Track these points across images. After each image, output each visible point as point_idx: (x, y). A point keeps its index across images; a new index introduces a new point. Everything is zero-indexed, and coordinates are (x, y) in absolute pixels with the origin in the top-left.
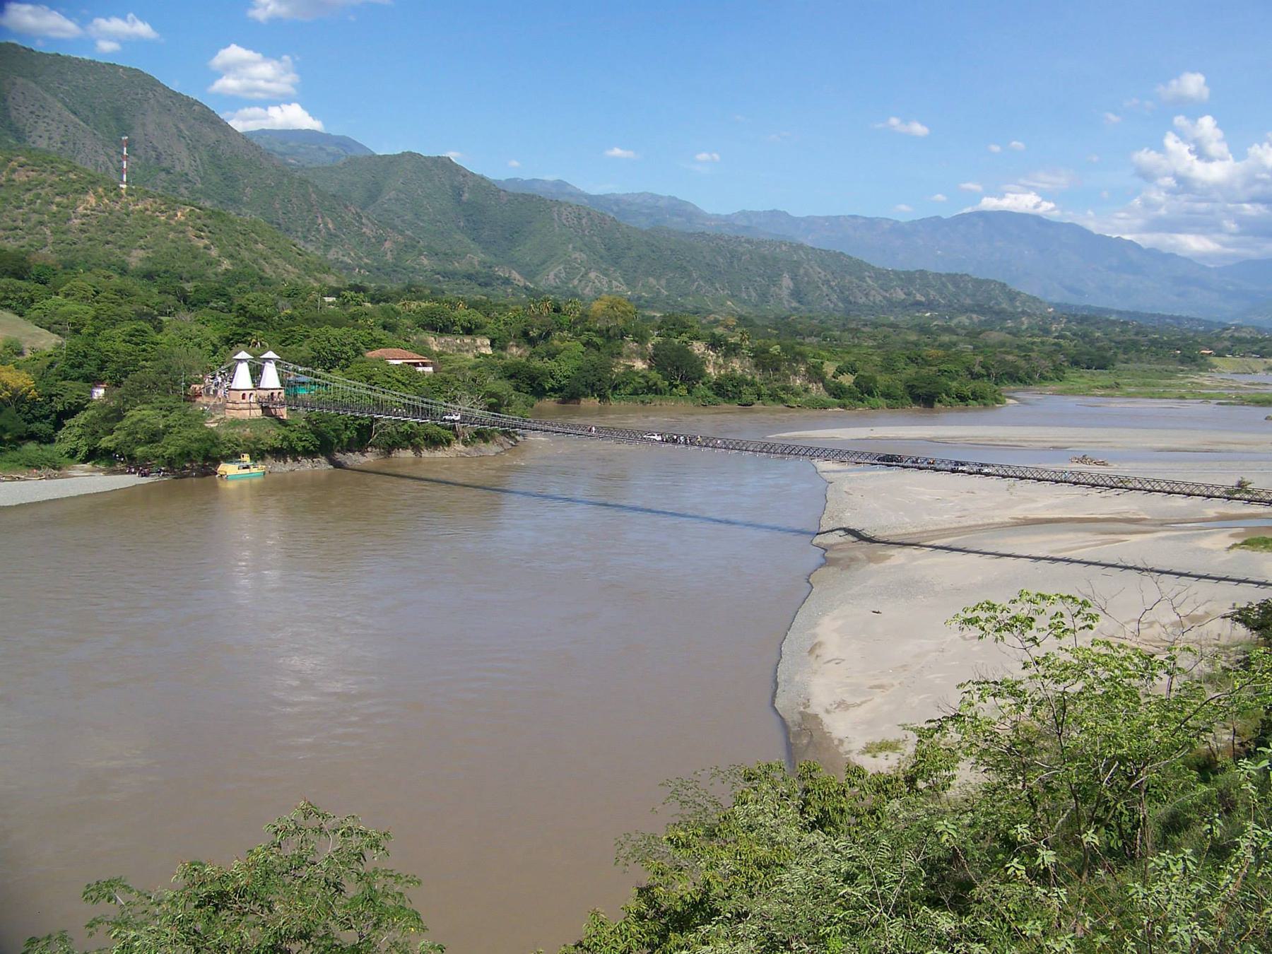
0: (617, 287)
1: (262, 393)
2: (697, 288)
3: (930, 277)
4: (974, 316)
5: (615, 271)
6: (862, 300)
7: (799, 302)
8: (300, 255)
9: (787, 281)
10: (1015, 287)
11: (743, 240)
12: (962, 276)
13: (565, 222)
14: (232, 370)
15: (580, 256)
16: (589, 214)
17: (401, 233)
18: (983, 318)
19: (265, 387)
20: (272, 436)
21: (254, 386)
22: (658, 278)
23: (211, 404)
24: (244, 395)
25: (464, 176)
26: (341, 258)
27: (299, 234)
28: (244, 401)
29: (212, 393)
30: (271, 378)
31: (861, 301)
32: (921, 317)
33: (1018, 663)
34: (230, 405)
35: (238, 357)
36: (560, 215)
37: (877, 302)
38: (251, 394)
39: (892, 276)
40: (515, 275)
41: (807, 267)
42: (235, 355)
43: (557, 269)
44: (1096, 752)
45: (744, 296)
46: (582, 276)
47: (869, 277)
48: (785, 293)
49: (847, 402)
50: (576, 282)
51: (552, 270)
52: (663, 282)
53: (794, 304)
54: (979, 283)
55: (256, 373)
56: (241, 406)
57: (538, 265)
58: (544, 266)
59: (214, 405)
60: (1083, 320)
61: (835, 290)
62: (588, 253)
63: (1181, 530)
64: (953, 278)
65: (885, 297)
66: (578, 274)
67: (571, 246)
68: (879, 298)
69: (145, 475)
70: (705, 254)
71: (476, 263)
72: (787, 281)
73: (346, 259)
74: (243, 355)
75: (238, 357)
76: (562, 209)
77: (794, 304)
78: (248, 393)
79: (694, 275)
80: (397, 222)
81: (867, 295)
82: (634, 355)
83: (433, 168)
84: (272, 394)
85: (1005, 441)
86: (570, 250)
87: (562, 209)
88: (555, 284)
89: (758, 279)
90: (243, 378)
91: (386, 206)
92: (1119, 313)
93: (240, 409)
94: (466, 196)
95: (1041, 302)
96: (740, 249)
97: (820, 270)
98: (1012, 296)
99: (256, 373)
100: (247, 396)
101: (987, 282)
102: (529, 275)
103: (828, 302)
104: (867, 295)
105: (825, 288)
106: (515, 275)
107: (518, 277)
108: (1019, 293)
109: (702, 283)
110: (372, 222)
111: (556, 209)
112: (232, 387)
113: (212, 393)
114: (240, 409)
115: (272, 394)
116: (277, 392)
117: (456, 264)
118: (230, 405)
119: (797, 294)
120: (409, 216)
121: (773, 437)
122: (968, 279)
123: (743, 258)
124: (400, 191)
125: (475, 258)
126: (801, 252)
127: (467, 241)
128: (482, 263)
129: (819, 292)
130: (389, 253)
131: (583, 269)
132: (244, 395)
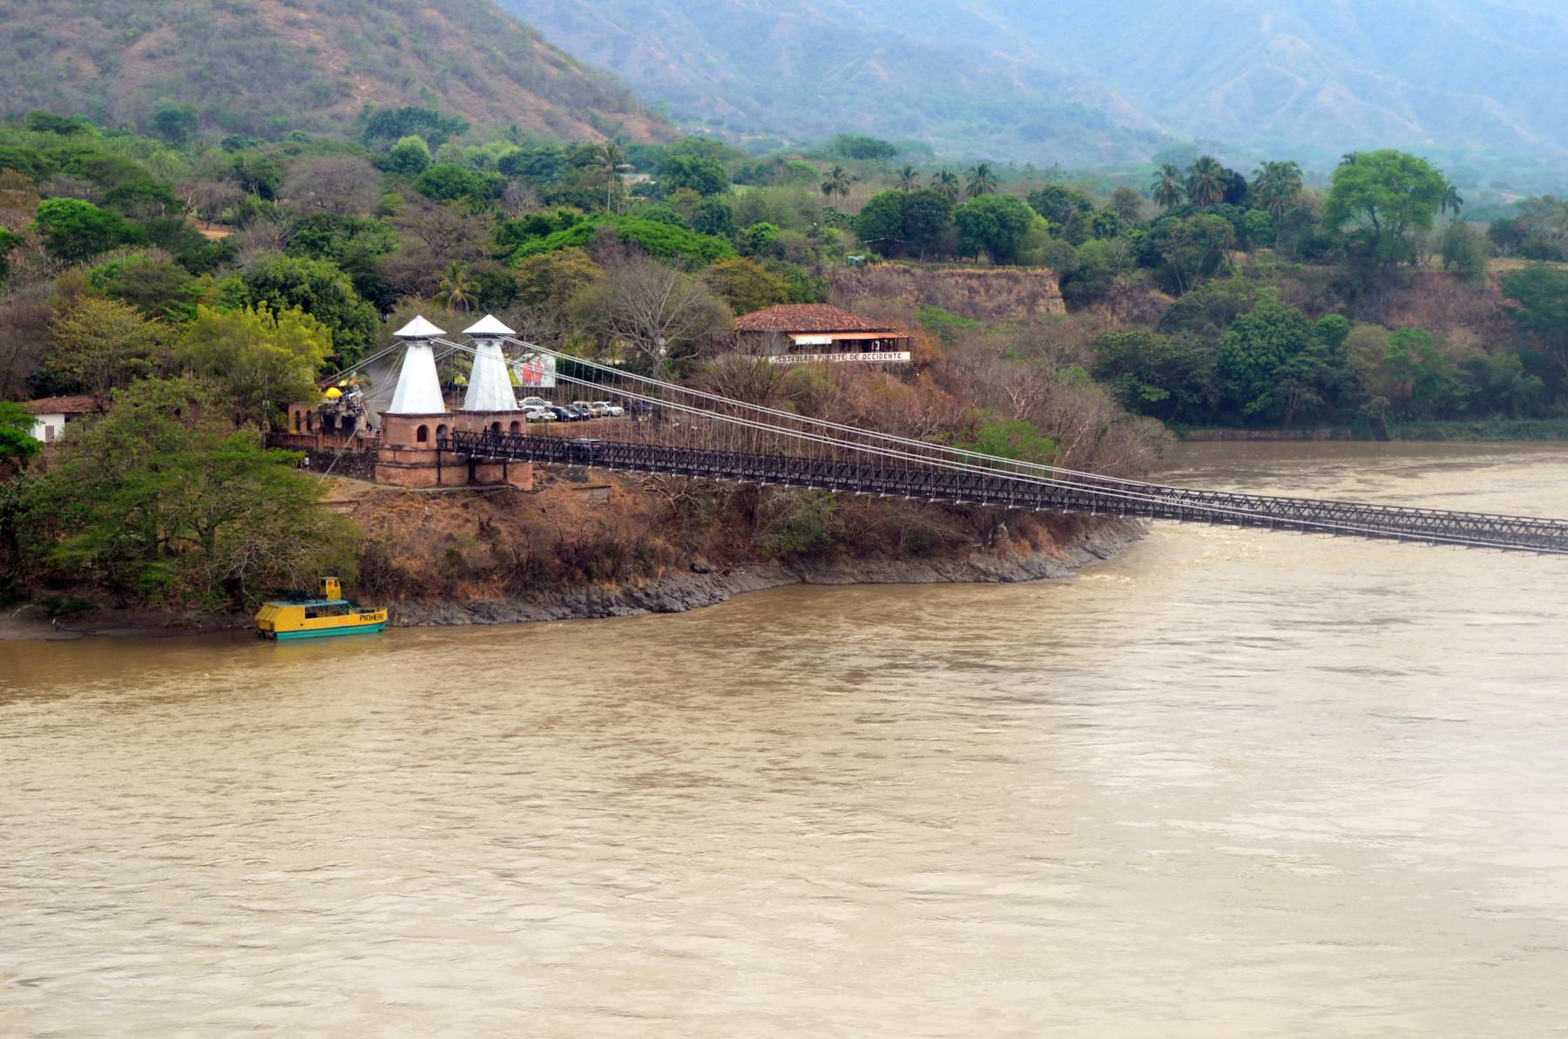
14: (392, 360)
19: (478, 407)
23: (339, 454)
27: (135, 451)
28: (422, 445)
29: (338, 425)
35: (406, 331)
42: (400, 327)
44: (1337, 286)
49: (1118, 335)
56: (415, 458)
59: (345, 457)
63: (1018, 920)
69: (119, 694)
74: (419, 326)
75: (406, 331)
82: (841, 548)
85: (926, 900)
100: (432, 431)
113: (338, 425)
115: (496, 426)
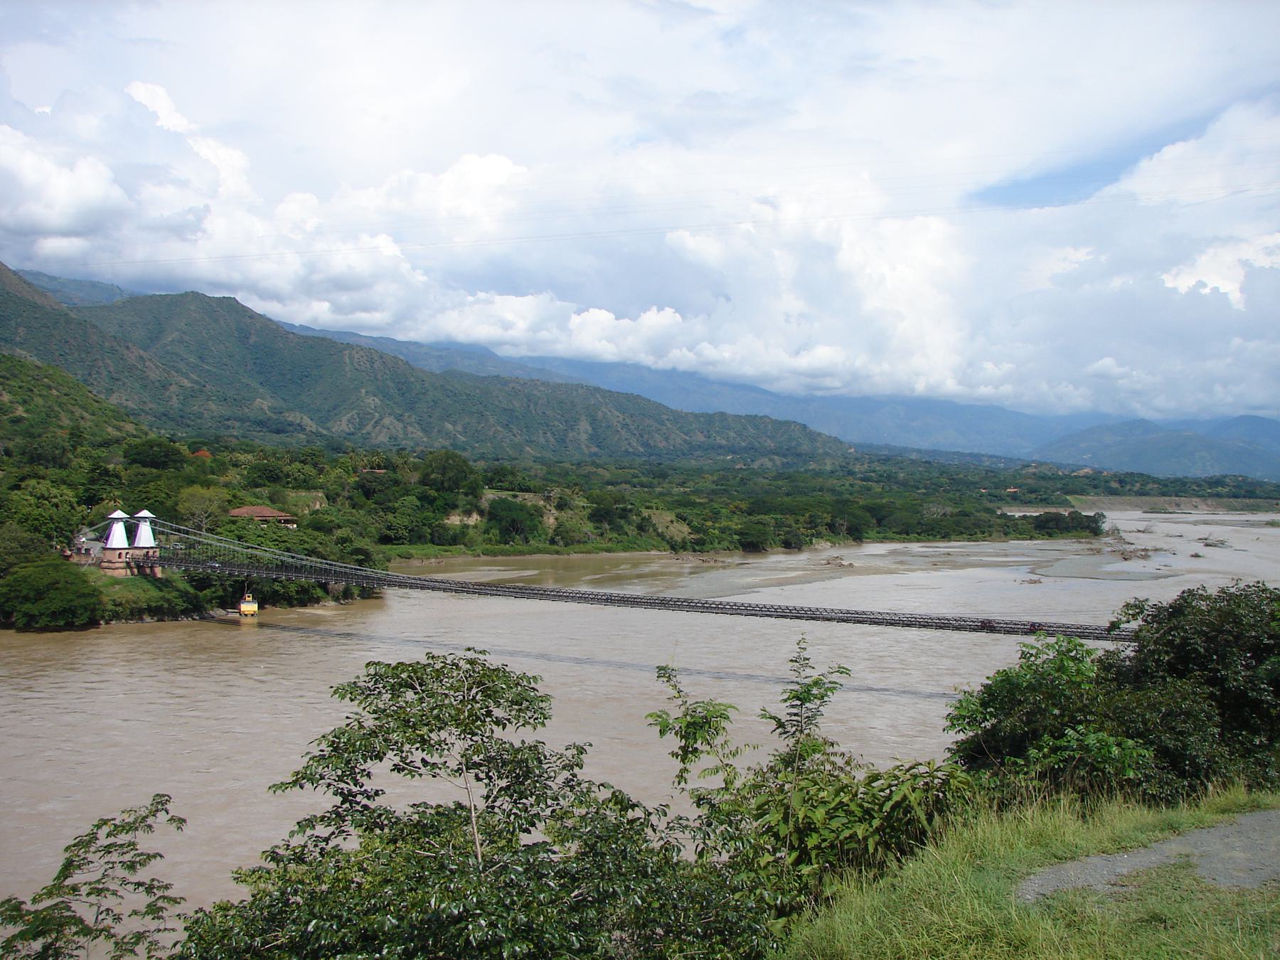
0: (412, 433)
1: (137, 552)
2: (494, 433)
3: (730, 419)
4: (776, 457)
5: (409, 417)
6: (662, 444)
7: (598, 446)
8: (97, 402)
9: (584, 426)
10: (814, 427)
11: (539, 383)
12: (761, 418)
13: (357, 366)
15: (372, 401)
16: (382, 358)
17: (187, 376)
18: (785, 460)
19: (141, 546)
20: (151, 594)
21: (129, 545)
22: (454, 424)
24: (120, 554)
25: (251, 317)
26: (125, 403)
28: (120, 560)
30: (146, 537)
31: (661, 445)
32: (723, 461)
33: (856, 675)
34: (106, 564)
36: (351, 358)
37: (677, 445)
38: (127, 553)
39: (691, 419)
40: (306, 421)
41: (606, 411)
43: (349, 415)
45: (542, 440)
46: (376, 422)
47: (667, 419)
48: (584, 437)
50: (369, 428)
51: (345, 415)
52: (459, 428)
53: (594, 449)
54: (779, 425)
55: (131, 532)
56: (117, 565)
57: (329, 411)
58: (335, 411)
60: (886, 460)
61: (635, 435)
62: (382, 398)
64: (752, 419)
65: (685, 441)
66: (371, 419)
67: (363, 391)
68: (679, 441)
70: (500, 398)
71: (266, 408)
72: (584, 426)
73: (130, 404)
76: (354, 352)
77: (594, 449)
78: (124, 552)
79: (491, 420)
80: (182, 365)
81: (667, 439)
83: (218, 309)
84: (148, 552)
86: (363, 395)
87: (354, 352)
88: (347, 430)
89: (556, 423)
90: (118, 537)
91: (169, 348)
92: (919, 451)
93: (117, 568)
94: (253, 339)
95: (841, 443)
96: (535, 392)
97: (618, 414)
98: (813, 436)
99: (131, 532)
100: (124, 555)
101: (788, 423)
102: (322, 421)
103: (628, 447)
104: (667, 439)
105: (623, 433)
106: (306, 421)
107: (310, 423)
108: (819, 434)
109: (499, 428)
110: (155, 365)
111: (347, 352)
112: (108, 547)
114: (117, 568)
116: (124, 552)
117: (247, 410)
118: (106, 564)
119: (595, 438)
120: (193, 359)
121: (569, 589)
122: (768, 421)
123: (540, 402)
124: (184, 333)
125: (264, 404)
126: (598, 396)
127: (254, 384)
128: (273, 409)
129: (618, 436)
130: (175, 399)
131: (377, 415)
132: (120, 554)
